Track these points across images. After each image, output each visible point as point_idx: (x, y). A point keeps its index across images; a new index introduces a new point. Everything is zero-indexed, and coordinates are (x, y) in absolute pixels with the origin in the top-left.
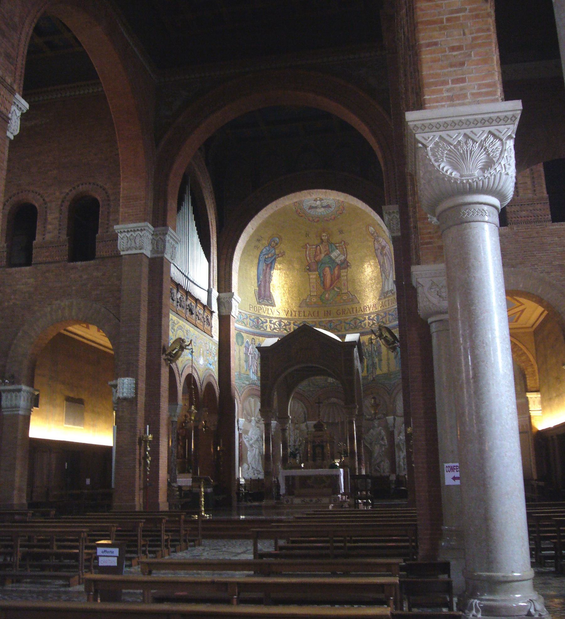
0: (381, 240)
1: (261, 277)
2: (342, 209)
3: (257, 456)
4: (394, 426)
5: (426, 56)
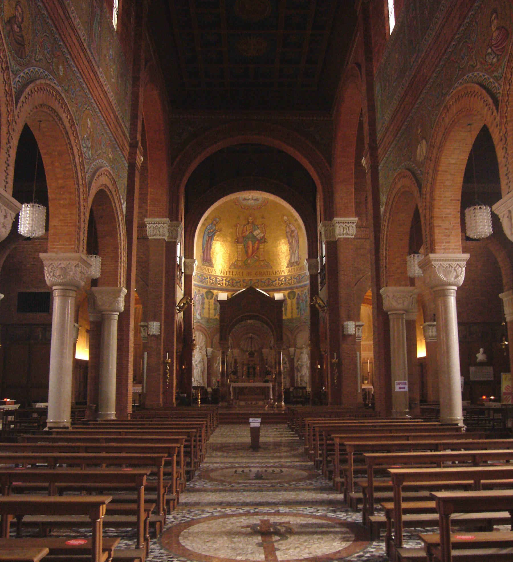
0: (292, 226)
1: (205, 246)
2: (266, 202)
3: (199, 373)
4: (294, 355)
5: (437, 231)
